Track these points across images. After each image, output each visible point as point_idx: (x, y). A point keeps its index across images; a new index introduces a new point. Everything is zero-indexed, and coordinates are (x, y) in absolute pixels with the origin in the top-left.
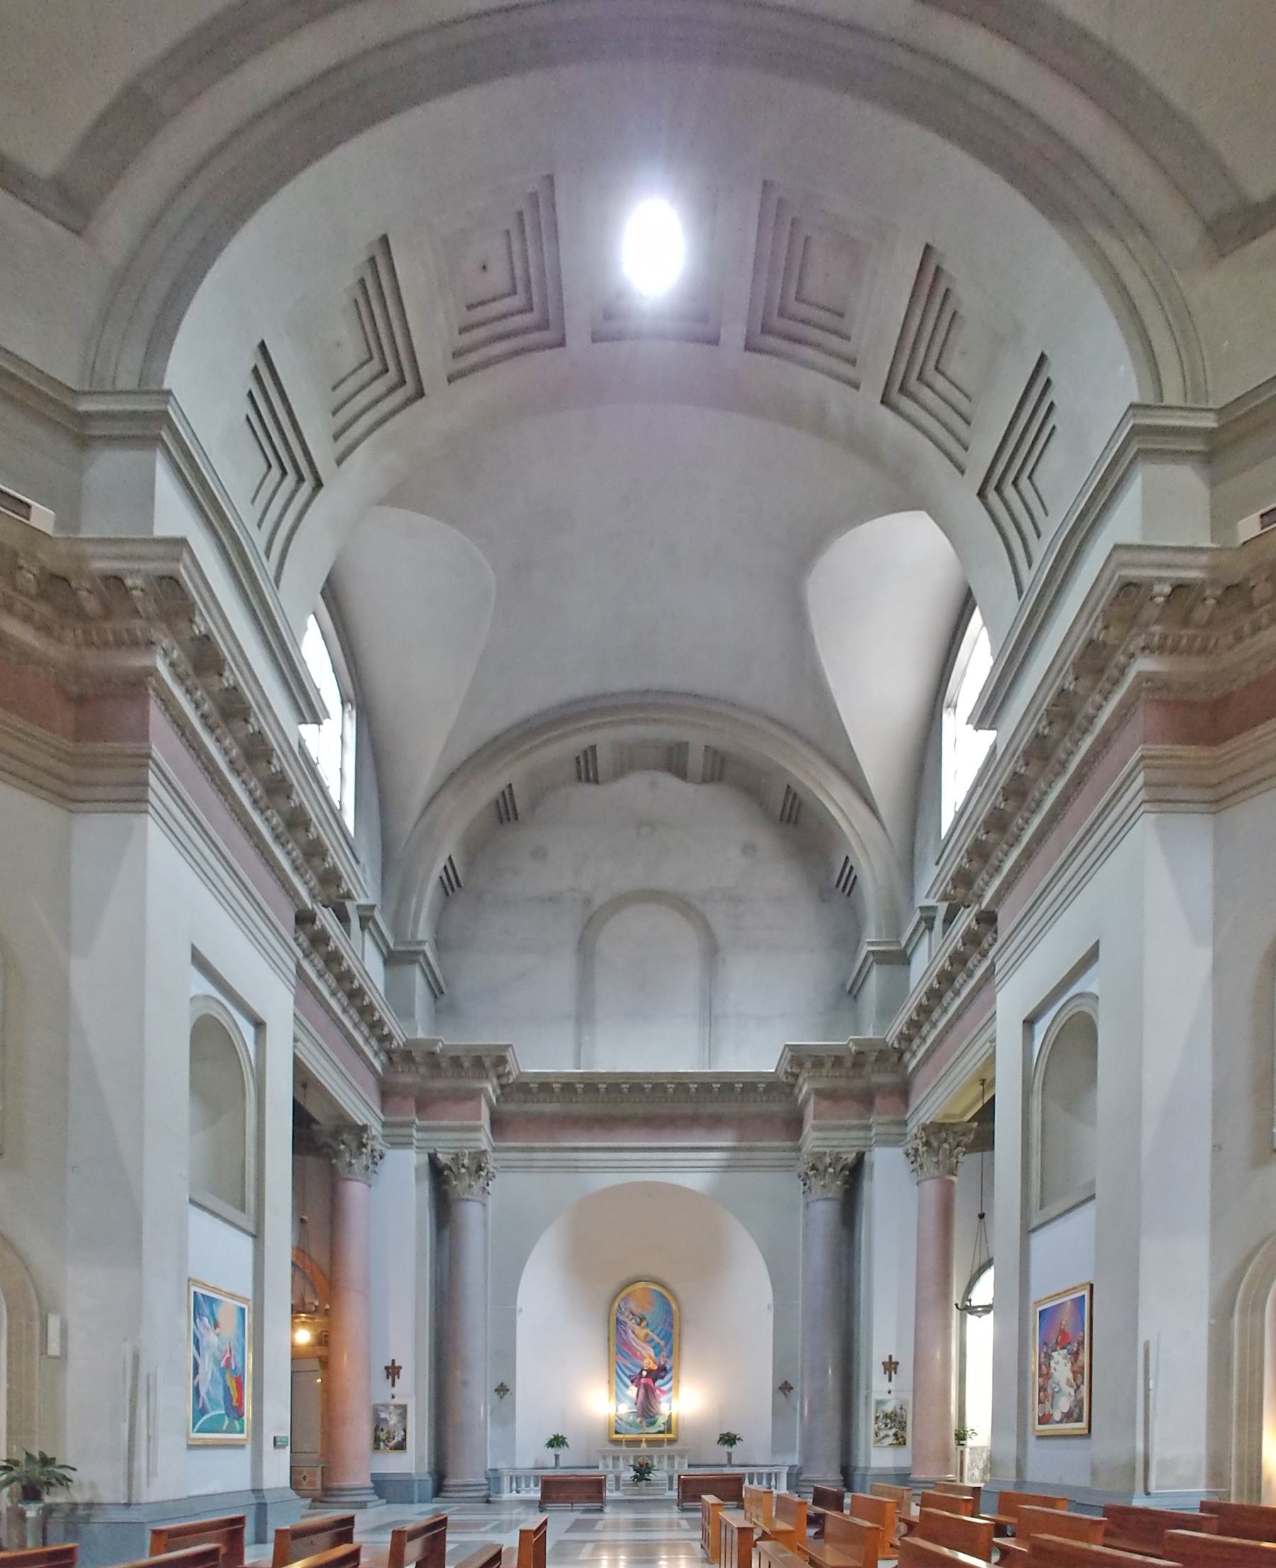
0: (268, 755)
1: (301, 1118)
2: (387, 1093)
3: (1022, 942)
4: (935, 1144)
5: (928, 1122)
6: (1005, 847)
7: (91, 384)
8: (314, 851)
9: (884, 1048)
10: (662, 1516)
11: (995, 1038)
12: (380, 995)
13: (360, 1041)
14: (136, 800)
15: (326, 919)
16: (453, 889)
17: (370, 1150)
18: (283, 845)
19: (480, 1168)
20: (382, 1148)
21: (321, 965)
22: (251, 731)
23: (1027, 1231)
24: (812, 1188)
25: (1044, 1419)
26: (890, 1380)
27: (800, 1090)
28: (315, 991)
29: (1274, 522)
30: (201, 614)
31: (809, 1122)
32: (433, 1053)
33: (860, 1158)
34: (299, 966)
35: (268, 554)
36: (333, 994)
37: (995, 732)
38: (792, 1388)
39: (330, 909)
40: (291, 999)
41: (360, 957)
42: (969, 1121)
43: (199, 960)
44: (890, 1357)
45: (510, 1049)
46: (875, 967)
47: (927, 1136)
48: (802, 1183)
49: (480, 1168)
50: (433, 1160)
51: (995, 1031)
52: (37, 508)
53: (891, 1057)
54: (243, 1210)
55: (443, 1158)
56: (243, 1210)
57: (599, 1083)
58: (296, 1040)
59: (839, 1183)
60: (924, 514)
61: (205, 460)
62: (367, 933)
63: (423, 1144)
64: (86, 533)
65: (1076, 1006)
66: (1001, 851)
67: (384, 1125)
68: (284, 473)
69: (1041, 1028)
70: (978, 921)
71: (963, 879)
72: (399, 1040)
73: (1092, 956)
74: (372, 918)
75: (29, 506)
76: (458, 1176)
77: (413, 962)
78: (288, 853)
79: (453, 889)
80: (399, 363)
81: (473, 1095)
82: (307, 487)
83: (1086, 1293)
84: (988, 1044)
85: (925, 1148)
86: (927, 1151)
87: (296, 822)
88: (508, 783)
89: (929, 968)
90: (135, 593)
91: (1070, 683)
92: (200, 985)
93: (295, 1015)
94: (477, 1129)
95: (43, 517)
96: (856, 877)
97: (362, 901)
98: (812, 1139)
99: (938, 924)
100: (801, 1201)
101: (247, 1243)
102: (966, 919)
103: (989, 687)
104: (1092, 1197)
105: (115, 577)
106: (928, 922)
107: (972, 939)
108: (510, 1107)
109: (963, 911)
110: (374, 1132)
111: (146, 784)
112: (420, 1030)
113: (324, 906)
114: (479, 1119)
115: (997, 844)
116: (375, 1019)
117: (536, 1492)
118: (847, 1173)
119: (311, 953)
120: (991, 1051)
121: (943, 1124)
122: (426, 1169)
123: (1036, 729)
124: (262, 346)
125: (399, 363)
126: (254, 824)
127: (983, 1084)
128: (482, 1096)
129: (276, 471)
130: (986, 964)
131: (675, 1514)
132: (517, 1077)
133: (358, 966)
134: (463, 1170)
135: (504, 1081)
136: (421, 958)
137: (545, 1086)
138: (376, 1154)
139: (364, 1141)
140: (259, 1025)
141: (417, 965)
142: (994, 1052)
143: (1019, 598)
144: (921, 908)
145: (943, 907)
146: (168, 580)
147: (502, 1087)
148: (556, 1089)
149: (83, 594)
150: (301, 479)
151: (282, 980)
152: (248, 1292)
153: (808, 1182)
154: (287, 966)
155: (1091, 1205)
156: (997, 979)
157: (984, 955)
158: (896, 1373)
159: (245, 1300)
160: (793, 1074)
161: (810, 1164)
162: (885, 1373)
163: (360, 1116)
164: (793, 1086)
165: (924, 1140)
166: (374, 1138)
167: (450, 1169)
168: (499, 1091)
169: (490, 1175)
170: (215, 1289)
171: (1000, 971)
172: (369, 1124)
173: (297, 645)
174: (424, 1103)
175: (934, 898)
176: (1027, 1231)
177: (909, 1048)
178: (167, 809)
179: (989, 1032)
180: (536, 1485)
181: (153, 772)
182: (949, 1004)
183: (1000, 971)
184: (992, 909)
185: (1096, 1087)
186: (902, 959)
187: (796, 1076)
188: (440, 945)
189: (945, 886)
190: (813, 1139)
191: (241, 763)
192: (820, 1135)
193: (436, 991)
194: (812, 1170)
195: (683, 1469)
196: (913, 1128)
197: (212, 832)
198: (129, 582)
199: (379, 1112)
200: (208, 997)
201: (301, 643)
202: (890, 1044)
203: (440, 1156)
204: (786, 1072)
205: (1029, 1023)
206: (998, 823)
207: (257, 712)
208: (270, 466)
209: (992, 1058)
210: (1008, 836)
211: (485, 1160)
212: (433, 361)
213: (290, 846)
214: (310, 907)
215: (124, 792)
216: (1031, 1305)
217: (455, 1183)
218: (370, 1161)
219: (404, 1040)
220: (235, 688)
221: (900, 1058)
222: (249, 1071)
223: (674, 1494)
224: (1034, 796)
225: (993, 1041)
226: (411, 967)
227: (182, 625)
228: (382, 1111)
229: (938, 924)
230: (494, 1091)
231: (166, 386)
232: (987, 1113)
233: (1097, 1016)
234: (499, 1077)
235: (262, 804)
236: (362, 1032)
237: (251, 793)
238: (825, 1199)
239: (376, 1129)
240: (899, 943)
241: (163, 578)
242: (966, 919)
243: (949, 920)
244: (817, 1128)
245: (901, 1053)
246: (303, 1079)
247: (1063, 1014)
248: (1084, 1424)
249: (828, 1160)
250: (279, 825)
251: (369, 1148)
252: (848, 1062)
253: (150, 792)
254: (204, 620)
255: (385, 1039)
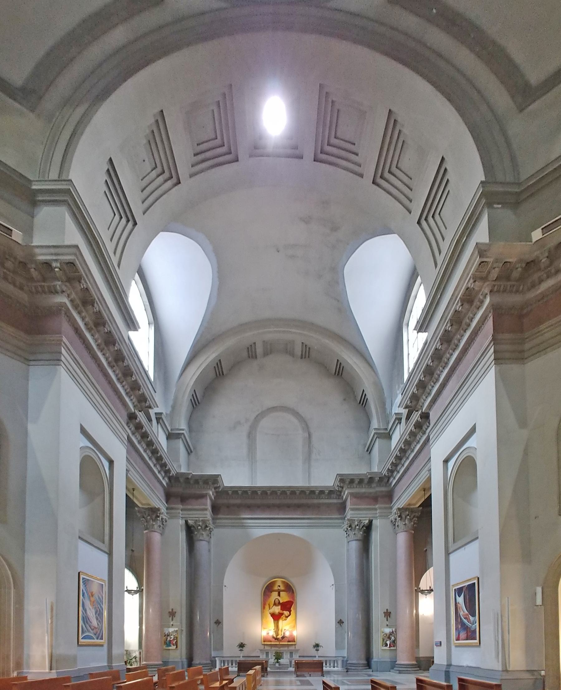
0: (123, 359)
1: (130, 504)
2: (169, 496)
3: (458, 402)
4: (403, 516)
5: (401, 507)
6: (451, 351)
7: (39, 178)
8: (135, 387)
9: (381, 476)
10: (287, 679)
11: (431, 469)
12: (165, 452)
13: (152, 465)
14: (57, 361)
15: (141, 417)
16: (196, 405)
17: (161, 519)
18: (130, 397)
19: (206, 526)
20: (166, 518)
21: (139, 438)
22: (106, 331)
23: (448, 554)
24: (350, 535)
25: (458, 639)
26: (387, 620)
27: (344, 493)
28: (137, 450)
29: (560, 225)
30: (97, 303)
31: (349, 505)
32: (188, 478)
33: (371, 522)
34: (128, 437)
35: (115, 253)
36: (145, 451)
37: (427, 333)
38: (343, 622)
39: (142, 412)
40: (125, 451)
41: (157, 436)
42: (418, 507)
43: (83, 431)
44: (387, 610)
45: (220, 476)
46: (377, 439)
47: (400, 513)
48: (346, 533)
49: (206, 526)
50: (186, 522)
51: (431, 466)
52: (14, 231)
53: (384, 480)
54: (104, 543)
55: (191, 522)
56: (104, 543)
57: (258, 491)
58: (127, 471)
59: (361, 533)
60: (396, 235)
61: (74, 189)
62: (159, 425)
63: (183, 516)
64: (35, 244)
65: (465, 454)
66: (433, 382)
67: (167, 509)
68: (121, 218)
69: (451, 464)
70: (421, 418)
71: (415, 398)
72: (173, 473)
73: (473, 431)
74: (161, 418)
75: (11, 230)
76: (198, 530)
77: (179, 438)
78: (123, 386)
79: (196, 405)
80: (169, 168)
81: (203, 496)
82: (130, 224)
83: (476, 581)
84: (428, 472)
85: (399, 518)
86: (400, 520)
87: (127, 373)
88: (219, 359)
89: (400, 439)
90: (56, 270)
91: (431, 363)
92: (85, 443)
93: (127, 457)
94: (206, 510)
95: (17, 235)
96: (367, 399)
97: (156, 410)
98: (349, 514)
99: (403, 421)
100: (346, 541)
101: (105, 557)
102: (416, 416)
103: (427, 305)
104: (477, 538)
105: (46, 263)
106: (400, 420)
107: (418, 426)
108: (220, 501)
109: (414, 413)
110: (162, 511)
111: (61, 353)
112: (182, 468)
113: (140, 411)
114: (207, 506)
115: (437, 366)
116: (167, 469)
117: (236, 667)
118: (365, 528)
119: (135, 433)
120: (429, 475)
121: (407, 508)
122: (184, 527)
123: (455, 308)
124: (111, 160)
125: (169, 168)
126: (118, 389)
127: (424, 491)
128: (208, 496)
129: (117, 216)
130: (424, 437)
131: (293, 678)
132: (223, 489)
133: (156, 439)
134: (199, 527)
135: (217, 490)
136: (182, 436)
137: (235, 491)
138: (164, 520)
139: (158, 515)
140: (111, 462)
141: (181, 439)
142: (431, 475)
143: (436, 267)
144: (396, 414)
145: (405, 412)
146: (70, 264)
147: (217, 492)
148: (240, 493)
149: (33, 270)
150: (128, 221)
151: (121, 443)
152: (106, 578)
153: (348, 533)
154: (124, 437)
155: (477, 541)
156: (431, 442)
157: (424, 433)
158: (390, 617)
159: (104, 581)
160: (341, 487)
161: (349, 525)
162: (385, 617)
163: (157, 504)
164: (341, 492)
165: (399, 515)
166: (162, 513)
167: (194, 527)
168: (215, 494)
169: (211, 529)
170: (92, 577)
171: (432, 438)
172: (160, 507)
173: (127, 297)
174: (184, 499)
175: (402, 407)
176: (448, 554)
177: (392, 475)
178: (68, 362)
179: (426, 468)
180: (236, 664)
181: (63, 346)
182: (414, 448)
183: (432, 438)
184: (427, 411)
185: (477, 488)
186: (389, 437)
187: (342, 488)
188: (190, 429)
189: (407, 401)
190: (350, 514)
191: (103, 346)
192: (353, 512)
193: (189, 452)
194: (350, 527)
195: (296, 657)
196: (394, 510)
197: (82, 363)
198: (54, 265)
199: (166, 504)
200: (88, 447)
201: (129, 291)
202: (384, 474)
203: (189, 521)
204: (338, 486)
205: (446, 461)
206: (429, 372)
207: (85, 277)
208: (115, 215)
209: (429, 479)
210: (452, 346)
211: (208, 523)
212: (183, 170)
213: (124, 383)
214: (133, 410)
215: (55, 362)
216: (451, 586)
217: (196, 533)
218: (161, 523)
219: (176, 473)
220: (87, 289)
221: (388, 480)
222: (106, 480)
223: (292, 669)
224: (444, 361)
225: (430, 470)
226: (177, 441)
227: (77, 284)
228: (167, 503)
229: (403, 421)
230: (213, 494)
231: (70, 178)
232: (427, 503)
233: (476, 457)
234: (215, 488)
235: (121, 380)
236: (152, 462)
237: (117, 376)
238: (356, 540)
239: (163, 510)
240: (386, 429)
241: (68, 263)
242: (416, 416)
243: (408, 418)
244: (352, 509)
245: (389, 478)
246: (131, 489)
247: (460, 458)
248: (477, 641)
249: (356, 523)
250: (127, 389)
251: (160, 518)
252: (366, 481)
253: (62, 357)
254: (86, 282)
255: (167, 472)
